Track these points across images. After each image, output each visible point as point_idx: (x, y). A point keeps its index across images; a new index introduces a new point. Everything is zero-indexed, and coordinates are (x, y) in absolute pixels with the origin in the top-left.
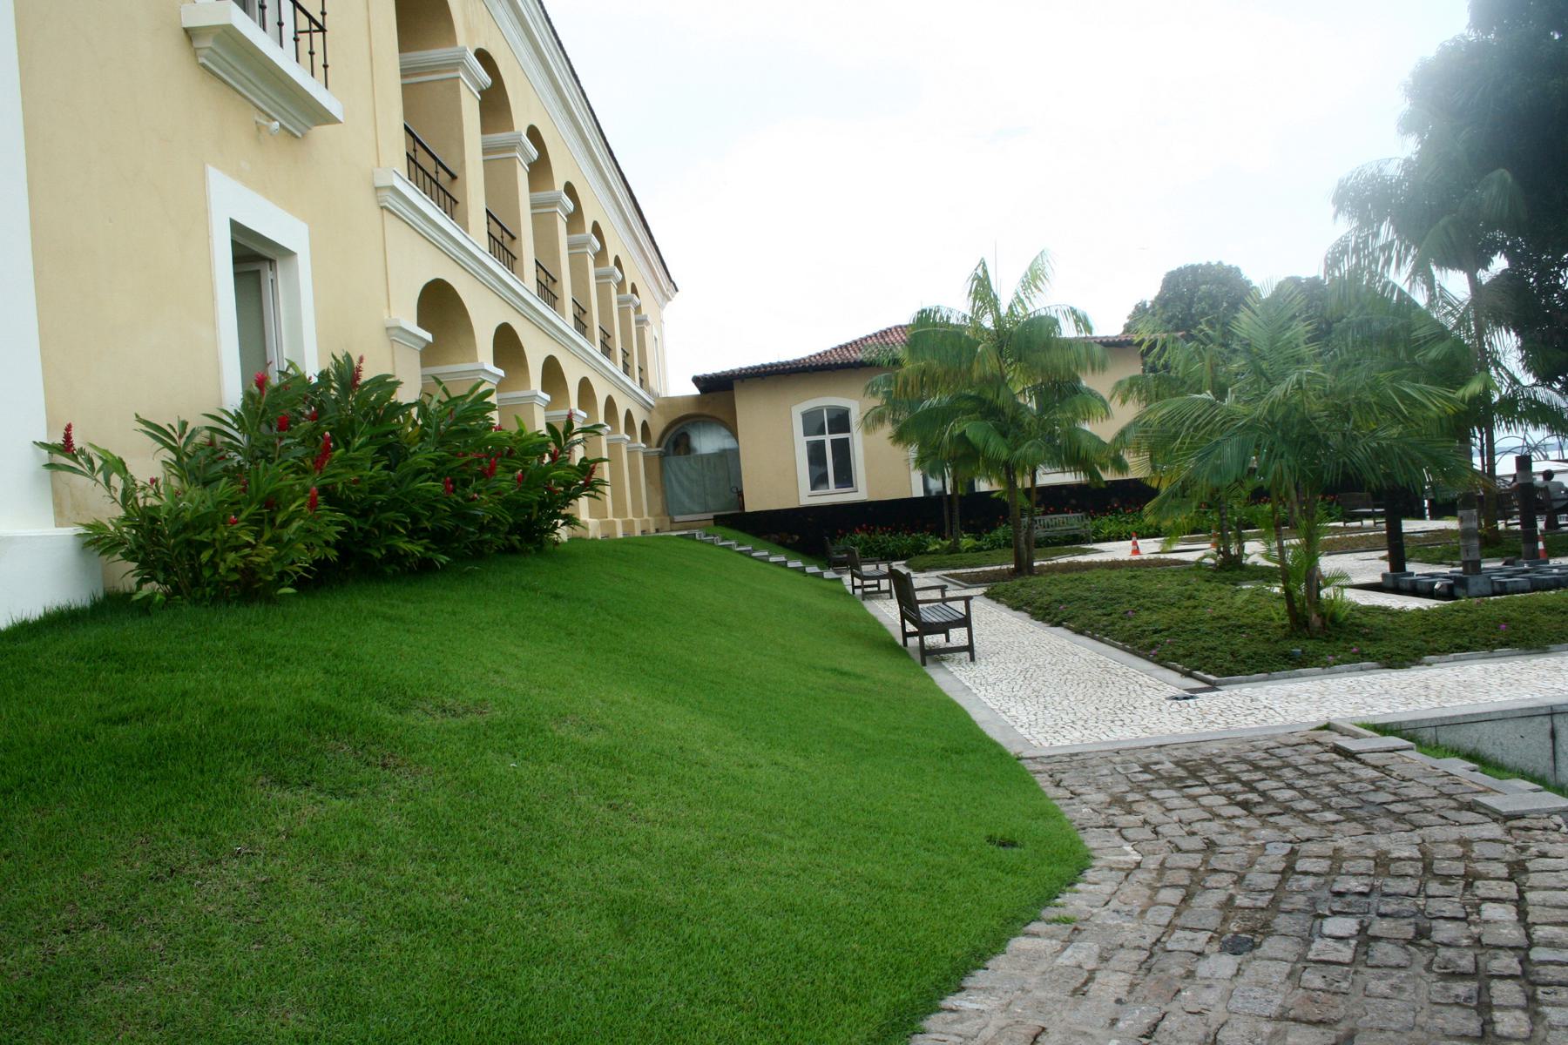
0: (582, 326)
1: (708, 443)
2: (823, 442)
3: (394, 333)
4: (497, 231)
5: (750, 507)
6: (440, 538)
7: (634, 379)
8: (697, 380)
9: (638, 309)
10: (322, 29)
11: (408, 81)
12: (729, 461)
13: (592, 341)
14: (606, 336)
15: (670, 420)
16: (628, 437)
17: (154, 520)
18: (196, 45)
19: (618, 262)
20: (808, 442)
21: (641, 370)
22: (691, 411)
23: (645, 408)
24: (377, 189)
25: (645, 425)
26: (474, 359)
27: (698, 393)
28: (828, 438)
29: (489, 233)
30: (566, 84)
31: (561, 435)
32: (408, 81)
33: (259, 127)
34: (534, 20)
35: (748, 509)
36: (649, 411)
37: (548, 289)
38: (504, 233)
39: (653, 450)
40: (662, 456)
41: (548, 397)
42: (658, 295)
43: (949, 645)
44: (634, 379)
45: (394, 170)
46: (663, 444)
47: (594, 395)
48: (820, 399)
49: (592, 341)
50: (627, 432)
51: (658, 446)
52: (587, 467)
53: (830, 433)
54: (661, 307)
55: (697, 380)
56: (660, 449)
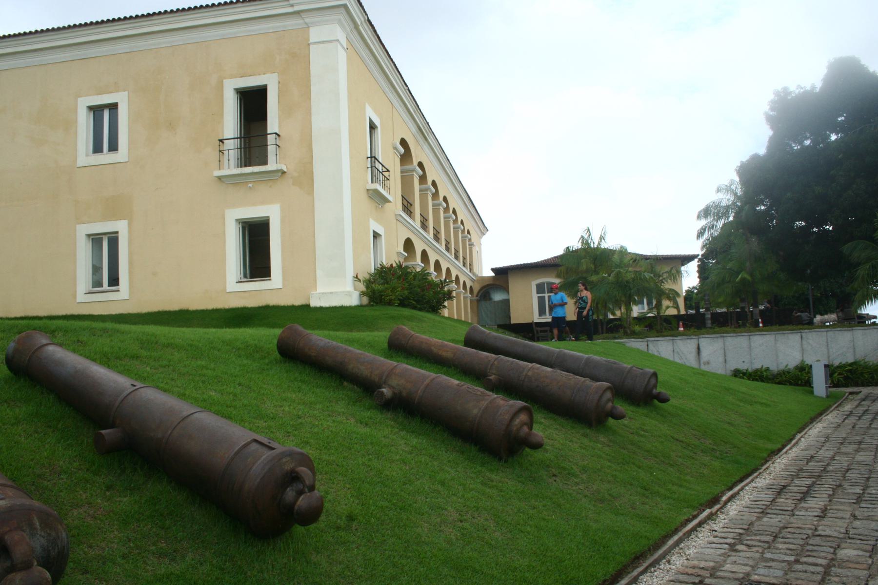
0: (448, 249)
1: (498, 297)
2: (544, 297)
3: (399, 254)
4: (405, 203)
5: (513, 321)
6: (418, 301)
7: (467, 268)
8: (493, 270)
9: (470, 240)
10: (389, 180)
11: (434, 208)
12: (506, 303)
13: (451, 254)
14: (457, 252)
15: (482, 286)
16: (464, 291)
17: (374, 290)
18: (369, 192)
19: (462, 222)
20: (538, 297)
21: (470, 265)
22: (491, 282)
23: (471, 280)
24: (396, 215)
25: (471, 288)
26: (416, 261)
27: (494, 275)
28: (546, 295)
29: (402, 203)
30: (445, 163)
31: (443, 283)
32: (445, 220)
33: (376, 206)
34: (435, 147)
35: (512, 323)
36: (473, 282)
37: (437, 238)
38: (408, 204)
39: (475, 298)
40: (478, 301)
41: (436, 274)
42: (480, 234)
43: (702, 365)
44: (467, 268)
45: (400, 211)
46: (479, 296)
47: (451, 274)
48: (547, 279)
49: (451, 254)
50: (463, 289)
51: (477, 296)
52: (450, 292)
53: (547, 293)
54: (481, 238)
55: (493, 270)
56: (477, 298)
